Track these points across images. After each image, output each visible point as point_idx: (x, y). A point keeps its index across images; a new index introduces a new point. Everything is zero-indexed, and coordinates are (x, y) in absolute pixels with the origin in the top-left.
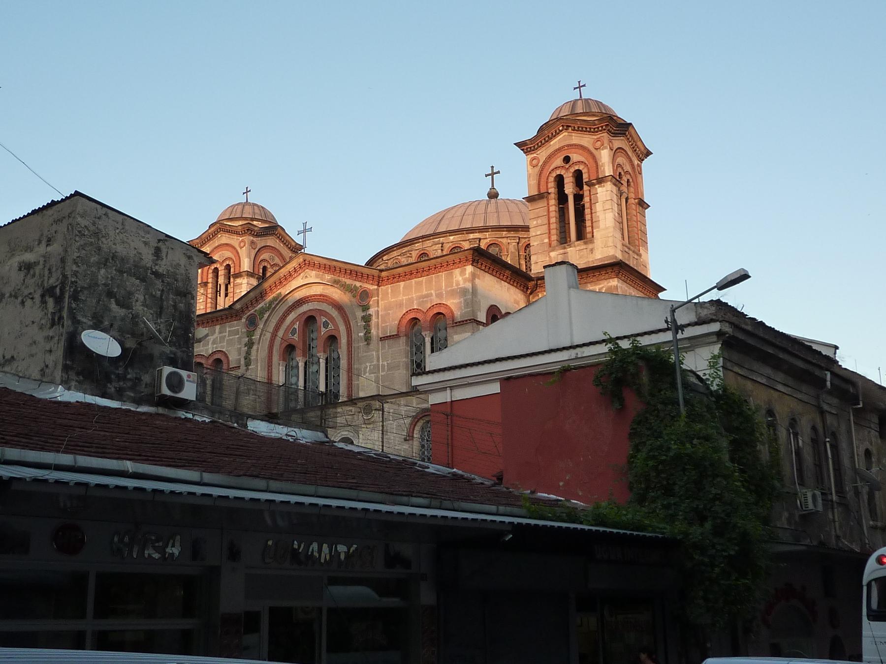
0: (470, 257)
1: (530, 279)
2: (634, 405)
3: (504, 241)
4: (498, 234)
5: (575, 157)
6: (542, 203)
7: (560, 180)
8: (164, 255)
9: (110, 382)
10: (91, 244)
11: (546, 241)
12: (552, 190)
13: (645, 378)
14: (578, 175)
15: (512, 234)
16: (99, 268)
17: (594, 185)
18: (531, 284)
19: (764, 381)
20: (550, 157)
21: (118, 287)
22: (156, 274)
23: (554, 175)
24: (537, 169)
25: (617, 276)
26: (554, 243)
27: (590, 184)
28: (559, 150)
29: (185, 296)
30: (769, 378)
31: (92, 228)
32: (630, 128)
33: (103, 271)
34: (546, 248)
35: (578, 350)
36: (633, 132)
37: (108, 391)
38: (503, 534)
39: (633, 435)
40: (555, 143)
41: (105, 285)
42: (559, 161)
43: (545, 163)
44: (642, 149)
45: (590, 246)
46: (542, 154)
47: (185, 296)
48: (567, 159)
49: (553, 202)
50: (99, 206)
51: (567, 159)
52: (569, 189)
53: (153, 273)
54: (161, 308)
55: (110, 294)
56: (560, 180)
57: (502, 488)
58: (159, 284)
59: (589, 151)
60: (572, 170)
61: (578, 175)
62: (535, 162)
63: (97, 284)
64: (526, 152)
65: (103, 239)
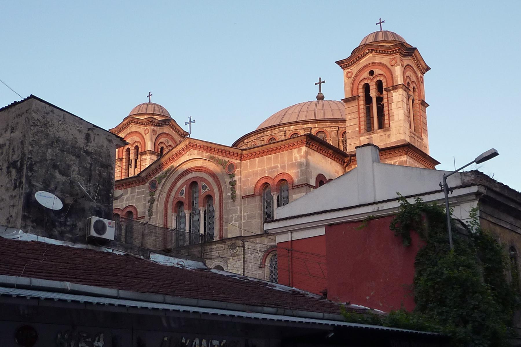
0: (304, 141)
1: (346, 156)
2: (418, 244)
3: (328, 129)
4: (324, 125)
5: (377, 71)
6: (354, 103)
7: (367, 88)
8: (92, 139)
9: (55, 227)
10: (42, 132)
11: (357, 129)
12: (362, 94)
13: (426, 224)
14: (379, 84)
15: (334, 125)
16: (47, 148)
17: (390, 90)
18: (347, 159)
19: (508, 226)
20: (360, 71)
21: (61, 161)
22: (87, 152)
23: (363, 83)
24: (351, 80)
25: (406, 154)
26: (363, 131)
27: (388, 90)
28: (366, 66)
29: (107, 167)
30: (511, 224)
31: (42, 120)
32: (415, 51)
33: (50, 150)
34: (357, 134)
35: (380, 205)
36: (417, 54)
37: (54, 233)
38: (327, 332)
39: (417, 264)
40: (364, 62)
41: (52, 160)
42: (366, 74)
43: (356, 75)
44: (424, 65)
45: (388, 133)
46: (355, 69)
47: (107, 167)
48: (372, 73)
49: (362, 102)
50: (47, 106)
51: (372, 73)
52: (373, 93)
53: (85, 152)
54: (90, 176)
55: (55, 166)
56: (367, 88)
57: (327, 301)
58: (89, 159)
59: (388, 69)
60: (375, 80)
61: (379, 84)
62: (349, 75)
63: (46, 160)
64: (344, 68)
65: (50, 128)
